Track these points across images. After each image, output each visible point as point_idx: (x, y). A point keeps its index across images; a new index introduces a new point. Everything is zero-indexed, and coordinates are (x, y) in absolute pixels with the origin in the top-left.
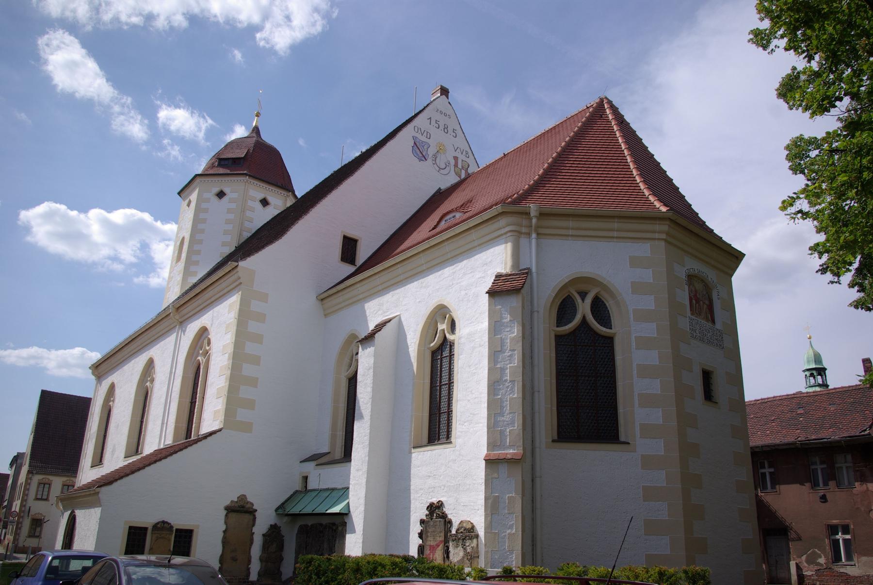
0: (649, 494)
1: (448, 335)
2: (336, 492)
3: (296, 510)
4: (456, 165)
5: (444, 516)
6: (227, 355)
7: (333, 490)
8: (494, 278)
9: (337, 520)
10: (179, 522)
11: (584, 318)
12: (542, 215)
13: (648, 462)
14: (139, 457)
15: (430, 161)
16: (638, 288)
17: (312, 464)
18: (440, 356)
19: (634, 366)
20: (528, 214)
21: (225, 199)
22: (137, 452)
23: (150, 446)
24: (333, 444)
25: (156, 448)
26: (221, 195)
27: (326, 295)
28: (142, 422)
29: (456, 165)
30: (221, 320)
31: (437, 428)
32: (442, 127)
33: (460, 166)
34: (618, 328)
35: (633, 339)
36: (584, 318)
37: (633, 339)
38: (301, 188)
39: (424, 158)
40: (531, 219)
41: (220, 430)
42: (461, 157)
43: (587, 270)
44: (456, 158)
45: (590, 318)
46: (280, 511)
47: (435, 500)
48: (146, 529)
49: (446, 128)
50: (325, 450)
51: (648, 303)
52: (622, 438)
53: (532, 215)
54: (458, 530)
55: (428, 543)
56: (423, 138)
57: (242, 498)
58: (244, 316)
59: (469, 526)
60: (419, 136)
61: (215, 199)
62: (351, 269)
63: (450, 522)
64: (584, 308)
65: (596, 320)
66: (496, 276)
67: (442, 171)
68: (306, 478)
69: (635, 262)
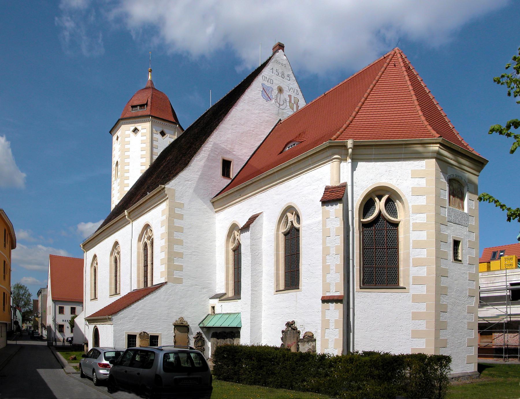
0: (416, 316)
1: (295, 225)
2: (232, 315)
3: (210, 325)
4: (290, 102)
5: (295, 329)
6: (164, 240)
7: (230, 314)
8: (324, 190)
9: (234, 331)
10: (151, 332)
11: (380, 212)
12: (356, 146)
13: (416, 299)
14: (117, 298)
15: (273, 101)
16: (416, 192)
17: (217, 300)
18: (292, 238)
19: (411, 241)
20: (345, 146)
21: (139, 134)
22: (116, 293)
23: (124, 291)
24: (227, 289)
25: (129, 291)
26: (135, 130)
27: (216, 199)
28: (116, 276)
29: (290, 102)
30: (156, 216)
31: (292, 279)
32: (280, 75)
33: (293, 102)
34: (401, 217)
35: (411, 224)
36: (380, 212)
37: (411, 224)
38: (187, 120)
39: (269, 99)
40: (347, 150)
41: (166, 283)
42: (293, 95)
43: (384, 181)
44: (290, 96)
45: (384, 212)
46: (201, 325)
47: (290, 320)
48: (136, 336)
49: (283, 74)
50: (223, 291)
51: (422, 201)
52: (401, 285)
53: (349, 147)
54: (304, 337)
55: (287, 343)
56: (269, 85)
57: (182, 319)
58: (173, 216)
59: (311, 335)
60: (266, 83)
61: (132, 134)
62: (227, 181)
63: (299, 332)
64: (380, 205)
65: (388, 213)
66: (326, 189)
67: (281, 107)
68: (213, 308)
69: (415, 175)
